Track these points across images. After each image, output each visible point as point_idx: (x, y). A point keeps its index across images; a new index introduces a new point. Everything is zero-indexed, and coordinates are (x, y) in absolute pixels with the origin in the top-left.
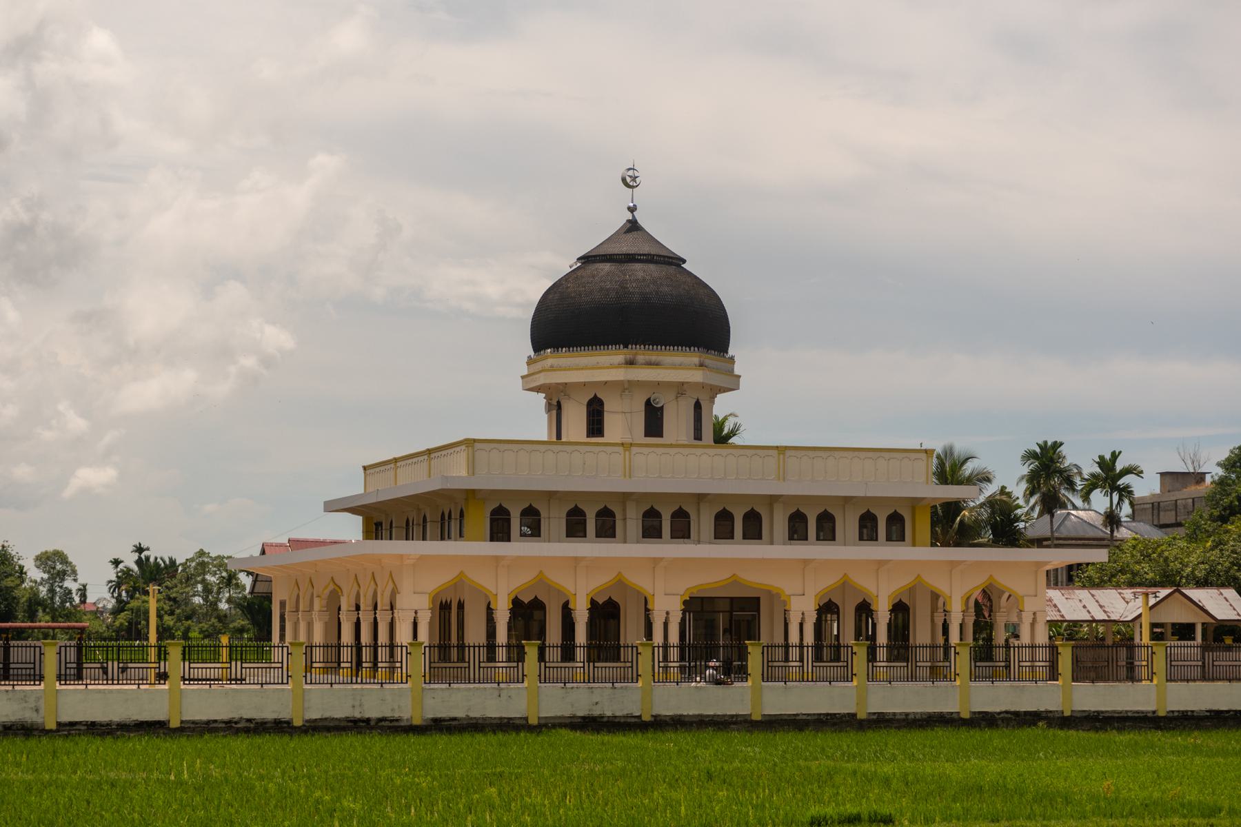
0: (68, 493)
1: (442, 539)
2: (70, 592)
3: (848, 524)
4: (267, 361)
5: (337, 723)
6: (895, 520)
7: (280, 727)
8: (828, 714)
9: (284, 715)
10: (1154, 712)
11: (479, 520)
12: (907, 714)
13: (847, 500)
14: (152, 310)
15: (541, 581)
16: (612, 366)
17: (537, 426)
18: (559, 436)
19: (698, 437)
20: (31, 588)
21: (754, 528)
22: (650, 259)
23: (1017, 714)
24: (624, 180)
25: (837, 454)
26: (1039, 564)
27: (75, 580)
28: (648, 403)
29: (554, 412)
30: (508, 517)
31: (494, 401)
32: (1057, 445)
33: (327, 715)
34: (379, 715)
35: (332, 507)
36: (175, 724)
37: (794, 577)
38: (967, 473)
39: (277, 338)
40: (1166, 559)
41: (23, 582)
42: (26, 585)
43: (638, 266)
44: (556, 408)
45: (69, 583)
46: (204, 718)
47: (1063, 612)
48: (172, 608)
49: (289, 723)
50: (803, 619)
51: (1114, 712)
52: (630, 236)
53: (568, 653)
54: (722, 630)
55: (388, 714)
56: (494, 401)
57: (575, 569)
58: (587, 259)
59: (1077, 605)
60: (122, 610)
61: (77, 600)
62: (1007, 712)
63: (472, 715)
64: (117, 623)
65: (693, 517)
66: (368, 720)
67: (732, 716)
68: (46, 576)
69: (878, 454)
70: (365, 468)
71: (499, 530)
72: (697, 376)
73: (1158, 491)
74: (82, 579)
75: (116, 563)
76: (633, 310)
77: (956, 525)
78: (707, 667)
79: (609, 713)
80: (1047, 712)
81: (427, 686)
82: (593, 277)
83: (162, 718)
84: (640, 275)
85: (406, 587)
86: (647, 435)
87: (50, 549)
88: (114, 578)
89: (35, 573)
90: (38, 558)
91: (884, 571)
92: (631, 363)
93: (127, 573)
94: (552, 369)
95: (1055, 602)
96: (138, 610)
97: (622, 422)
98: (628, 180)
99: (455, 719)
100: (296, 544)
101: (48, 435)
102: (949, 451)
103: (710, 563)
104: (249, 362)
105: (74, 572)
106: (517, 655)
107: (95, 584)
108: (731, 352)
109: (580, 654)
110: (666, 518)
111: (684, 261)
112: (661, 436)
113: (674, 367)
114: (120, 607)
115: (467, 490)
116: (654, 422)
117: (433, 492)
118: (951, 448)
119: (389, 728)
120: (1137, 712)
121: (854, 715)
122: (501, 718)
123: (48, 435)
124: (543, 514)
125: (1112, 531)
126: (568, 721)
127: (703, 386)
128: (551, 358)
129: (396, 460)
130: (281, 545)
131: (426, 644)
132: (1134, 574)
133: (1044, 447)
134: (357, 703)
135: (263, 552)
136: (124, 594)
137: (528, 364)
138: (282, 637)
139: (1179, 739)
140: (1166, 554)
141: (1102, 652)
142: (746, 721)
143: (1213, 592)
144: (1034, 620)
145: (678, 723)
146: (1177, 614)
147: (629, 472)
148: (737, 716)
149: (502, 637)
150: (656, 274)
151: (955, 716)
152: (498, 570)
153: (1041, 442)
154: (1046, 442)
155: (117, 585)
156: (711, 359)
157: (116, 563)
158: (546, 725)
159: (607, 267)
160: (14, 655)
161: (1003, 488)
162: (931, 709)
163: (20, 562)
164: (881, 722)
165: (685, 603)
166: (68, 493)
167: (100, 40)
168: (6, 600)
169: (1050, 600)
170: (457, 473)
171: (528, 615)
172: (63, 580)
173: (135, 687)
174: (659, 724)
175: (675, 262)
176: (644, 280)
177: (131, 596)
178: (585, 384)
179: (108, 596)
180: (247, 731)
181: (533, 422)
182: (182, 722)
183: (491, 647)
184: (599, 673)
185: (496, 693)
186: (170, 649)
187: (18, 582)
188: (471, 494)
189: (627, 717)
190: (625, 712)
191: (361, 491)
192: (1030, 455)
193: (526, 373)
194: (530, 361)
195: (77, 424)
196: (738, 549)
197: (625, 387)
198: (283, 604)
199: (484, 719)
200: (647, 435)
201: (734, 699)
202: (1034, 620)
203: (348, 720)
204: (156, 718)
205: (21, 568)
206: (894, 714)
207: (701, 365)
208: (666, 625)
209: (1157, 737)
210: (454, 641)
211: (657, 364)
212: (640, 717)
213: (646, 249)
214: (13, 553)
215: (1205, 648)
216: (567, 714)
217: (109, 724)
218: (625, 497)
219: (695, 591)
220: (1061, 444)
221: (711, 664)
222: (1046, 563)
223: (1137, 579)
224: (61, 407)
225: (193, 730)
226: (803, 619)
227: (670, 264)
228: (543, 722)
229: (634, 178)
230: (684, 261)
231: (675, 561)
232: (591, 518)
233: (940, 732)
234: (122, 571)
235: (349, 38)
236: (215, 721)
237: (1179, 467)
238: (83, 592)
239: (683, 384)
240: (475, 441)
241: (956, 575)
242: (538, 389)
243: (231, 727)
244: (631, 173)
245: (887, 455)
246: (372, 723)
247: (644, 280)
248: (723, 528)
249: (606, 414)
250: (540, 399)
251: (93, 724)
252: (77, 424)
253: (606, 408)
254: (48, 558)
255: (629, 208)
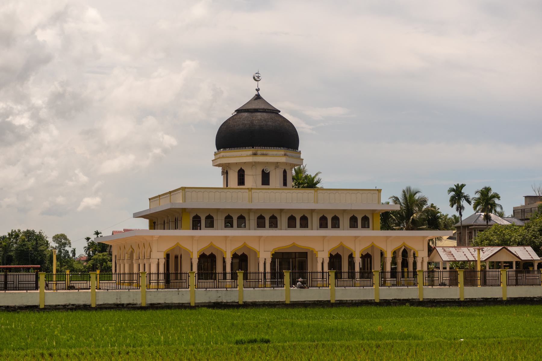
0: (80, 209)
1: (176, 229)
2: (68, 252)
3: (345, 221)
4: (165, 151)
5: (110, 306)
6: (365, 220)
7: (86, 308)
8: (318, 301)
9: (88, 303)
10: (459, 299)
11: (188, 220)
12: (352, 301)
13: (344, 211)
14: (116, 129)
15: (211, 246)
16: (247, 156)
17: (218, 181)
18: (227, 186)
19: (285, 184)
20: (51, 250)
21: (304, 223)
22: (264, 111)
23: (399, 300)
24: (254, 78)
25: (340, 192)
26: (424, 237)
27: (70, 247)
28: (263, 171)
29: (225, 175)
30: (201, 219)
31: (202, 171)
32: (463, 186)
33: (106, 302)
34: (128, 302)
35: (137, 215)
36: (42, 306)
37: (320, 244)
38: (417, 198)
39: (169, 140)
40: (504, 234)
41: (48, 248)
42: (49, 249)
43: (259, 114)
44: (225, 173)
45: (67, 248)
46: (54, 304)
47: (455, 257)
48: (101, 257)
49: (90, 306)
50: (323, 261)
51: (441, 299)
52: (256, 101)
53: (352, 275)
54: (292, 264)
55: (131, 302)
56: (202, 171)
57: (226, 241)
58: (238, 111)
59: (466, 254)
60: (90, 260)
61: (71, 255)
62: (395, 299)
63: (167, 302)
64: (88, 265)
65: (279, 219)
66: (123, 305)
67: (277, 302)
68: (57, 245)
69: (357, 191)
70: (150, 199)
71: (196, 224)
72: (283, 160)
73: (524, 204)
74: (73, 246)
75: (88, 239)
76: (257, 132)
77: (411, 220)
78: (298, 281)
79: (225, 301)
80: (412, 299)
81: (148, 290)
82: (240, 118)
83: (36, 304)
84: (259, 117)
85: (154, 249)
86: (263, 184)
87: (59, 233)
88: (87, 246)
89: (53, 244)
90: (54, 237)
91: (356, 241)
92: (255, 154)
93: (93, 243)
94: (223, 157)
95: (452, 253)
96: (97, 259)
97: (253, 179)
98: (256, 78)
99: (159, 304)
100: (125, 230)
101: (71, 184)
102: (409, 189)
103: (285, 237)
104: (157, 151)
105: (70, 243)
106: (234, 277)
107: (79, 248)
108: (299, 149)
109: (358, 275)
110: (267, 219)
111: (280, 112)
112: (269, 184)
113: (273, 156)
114: (89, 258)
115: (182, 209)
116: (266, 179)
117: (163, 211)
118: (410, 188)
119: (132, 307)
120: (452, 299)
121: (329, 301)
122: (179, 303)
123: (71, 184)
124: (215, 218)
125: (487, 222)
126: (207, 304)
127: (286, 164)
128: (225, 153)
129: (159, 196)
130: (120, 232)
131: (148, 273)
132: (491, 241)
133: (457, 186)
134: (118, 297)
135: (113, 234)
136: (91, 252)
137: (215, 155)
138: (116, 271)
139: (431, 309)
140: (504, 232)
141: (469, 272)
142: (283, 304)
143: (521, 248)
144: (423, 261)
145: (254, 305)
146: (504, 258)
147: (251, 200)
148: (279, 302)
149: (228, 269)
150: (266, 117)
151: (373, 301)
152: (193, 242)
153: (456, 184)
154: (458, 184)
155: (88, 249)
156: (290, 152)
157: (88, 239)
158: (198, 306)
159: (246, 114)
160: (10, 278)
161: (432, 204)
162: (362, 299)
163: (47, 239)
164: (341, 304)
165: (273, 255)
166: (80, 209)
167: (92, 13)
168: (40, 255)
169: (450, 252)
170: (178, 202)
171: (241, 260)
172: (65, 247)
173: (25, 291)
174: (246, 305)
175: (276, 112)
176: (261, 120)
177: (94, 254)
178: (236, 163)
179: (84, 253)
180: (72, 309)
181: (216, 179)
182: (45, 306)
183: (225, 274)
184: (200, 284)
185: (177, 293)
186: (91, 276)
187: (46, 248)
188: (184, 210)
189: (232, 302)
190: (232, 301)
191: (149, 208)
192: (452, 190)
193: (214, 158)
194: (216, 154)
195: (83, 179)
196: (298, 232)
197: (254, 165)
198: (116, 256)
199: (172, 304)
200: (263, 184)
201: (297, 294)
202: (423, 261)
203: (114, 304)
204: (34, 304)
205: (47, 242)
206: (347, 300)
207: (285, 155)
208: (265, 264)
209: (460, 310)
210: (179, 272)
211: (266, 155)
212: (238, 302)
213: (263, 106)
214: (44, 235)
215: (517, 272)
216: (207, 301)
217: (14, 307)
218: (249, 211)
219: (277, 250)
220: (463, 186)
221: (299, 280)
222: (427, 237)
223: (492, 243)
224: (76, 172)
225: (50, 309)
226: (323, 261)
227: (273, 113)
228: (197, 305)
229: (258, 77)
230: (280, 112)
231: (267, 237)
232: (234, 219)
233: (364, 308)
234: (90, 242)
235: (199, 11)
236: (59, 305)
237: (533, 194)
238: (74, 252)
239: (277, 163)
240: (185, 188)
241: (389, 241)
242: (219, 165)
243: (65, 308)
244: (257, 75)
245: (361, 192)
246: (125, 306)
247: (261, 120)
248: (291, 223)
249: (246, 177)
250: (220, 169)
251: (8, 307)
252: (83, 179)
253: (246, 173)
254: (58, 237)
255: (256, 90)
